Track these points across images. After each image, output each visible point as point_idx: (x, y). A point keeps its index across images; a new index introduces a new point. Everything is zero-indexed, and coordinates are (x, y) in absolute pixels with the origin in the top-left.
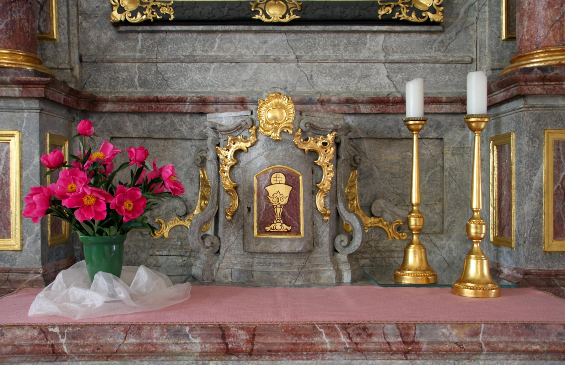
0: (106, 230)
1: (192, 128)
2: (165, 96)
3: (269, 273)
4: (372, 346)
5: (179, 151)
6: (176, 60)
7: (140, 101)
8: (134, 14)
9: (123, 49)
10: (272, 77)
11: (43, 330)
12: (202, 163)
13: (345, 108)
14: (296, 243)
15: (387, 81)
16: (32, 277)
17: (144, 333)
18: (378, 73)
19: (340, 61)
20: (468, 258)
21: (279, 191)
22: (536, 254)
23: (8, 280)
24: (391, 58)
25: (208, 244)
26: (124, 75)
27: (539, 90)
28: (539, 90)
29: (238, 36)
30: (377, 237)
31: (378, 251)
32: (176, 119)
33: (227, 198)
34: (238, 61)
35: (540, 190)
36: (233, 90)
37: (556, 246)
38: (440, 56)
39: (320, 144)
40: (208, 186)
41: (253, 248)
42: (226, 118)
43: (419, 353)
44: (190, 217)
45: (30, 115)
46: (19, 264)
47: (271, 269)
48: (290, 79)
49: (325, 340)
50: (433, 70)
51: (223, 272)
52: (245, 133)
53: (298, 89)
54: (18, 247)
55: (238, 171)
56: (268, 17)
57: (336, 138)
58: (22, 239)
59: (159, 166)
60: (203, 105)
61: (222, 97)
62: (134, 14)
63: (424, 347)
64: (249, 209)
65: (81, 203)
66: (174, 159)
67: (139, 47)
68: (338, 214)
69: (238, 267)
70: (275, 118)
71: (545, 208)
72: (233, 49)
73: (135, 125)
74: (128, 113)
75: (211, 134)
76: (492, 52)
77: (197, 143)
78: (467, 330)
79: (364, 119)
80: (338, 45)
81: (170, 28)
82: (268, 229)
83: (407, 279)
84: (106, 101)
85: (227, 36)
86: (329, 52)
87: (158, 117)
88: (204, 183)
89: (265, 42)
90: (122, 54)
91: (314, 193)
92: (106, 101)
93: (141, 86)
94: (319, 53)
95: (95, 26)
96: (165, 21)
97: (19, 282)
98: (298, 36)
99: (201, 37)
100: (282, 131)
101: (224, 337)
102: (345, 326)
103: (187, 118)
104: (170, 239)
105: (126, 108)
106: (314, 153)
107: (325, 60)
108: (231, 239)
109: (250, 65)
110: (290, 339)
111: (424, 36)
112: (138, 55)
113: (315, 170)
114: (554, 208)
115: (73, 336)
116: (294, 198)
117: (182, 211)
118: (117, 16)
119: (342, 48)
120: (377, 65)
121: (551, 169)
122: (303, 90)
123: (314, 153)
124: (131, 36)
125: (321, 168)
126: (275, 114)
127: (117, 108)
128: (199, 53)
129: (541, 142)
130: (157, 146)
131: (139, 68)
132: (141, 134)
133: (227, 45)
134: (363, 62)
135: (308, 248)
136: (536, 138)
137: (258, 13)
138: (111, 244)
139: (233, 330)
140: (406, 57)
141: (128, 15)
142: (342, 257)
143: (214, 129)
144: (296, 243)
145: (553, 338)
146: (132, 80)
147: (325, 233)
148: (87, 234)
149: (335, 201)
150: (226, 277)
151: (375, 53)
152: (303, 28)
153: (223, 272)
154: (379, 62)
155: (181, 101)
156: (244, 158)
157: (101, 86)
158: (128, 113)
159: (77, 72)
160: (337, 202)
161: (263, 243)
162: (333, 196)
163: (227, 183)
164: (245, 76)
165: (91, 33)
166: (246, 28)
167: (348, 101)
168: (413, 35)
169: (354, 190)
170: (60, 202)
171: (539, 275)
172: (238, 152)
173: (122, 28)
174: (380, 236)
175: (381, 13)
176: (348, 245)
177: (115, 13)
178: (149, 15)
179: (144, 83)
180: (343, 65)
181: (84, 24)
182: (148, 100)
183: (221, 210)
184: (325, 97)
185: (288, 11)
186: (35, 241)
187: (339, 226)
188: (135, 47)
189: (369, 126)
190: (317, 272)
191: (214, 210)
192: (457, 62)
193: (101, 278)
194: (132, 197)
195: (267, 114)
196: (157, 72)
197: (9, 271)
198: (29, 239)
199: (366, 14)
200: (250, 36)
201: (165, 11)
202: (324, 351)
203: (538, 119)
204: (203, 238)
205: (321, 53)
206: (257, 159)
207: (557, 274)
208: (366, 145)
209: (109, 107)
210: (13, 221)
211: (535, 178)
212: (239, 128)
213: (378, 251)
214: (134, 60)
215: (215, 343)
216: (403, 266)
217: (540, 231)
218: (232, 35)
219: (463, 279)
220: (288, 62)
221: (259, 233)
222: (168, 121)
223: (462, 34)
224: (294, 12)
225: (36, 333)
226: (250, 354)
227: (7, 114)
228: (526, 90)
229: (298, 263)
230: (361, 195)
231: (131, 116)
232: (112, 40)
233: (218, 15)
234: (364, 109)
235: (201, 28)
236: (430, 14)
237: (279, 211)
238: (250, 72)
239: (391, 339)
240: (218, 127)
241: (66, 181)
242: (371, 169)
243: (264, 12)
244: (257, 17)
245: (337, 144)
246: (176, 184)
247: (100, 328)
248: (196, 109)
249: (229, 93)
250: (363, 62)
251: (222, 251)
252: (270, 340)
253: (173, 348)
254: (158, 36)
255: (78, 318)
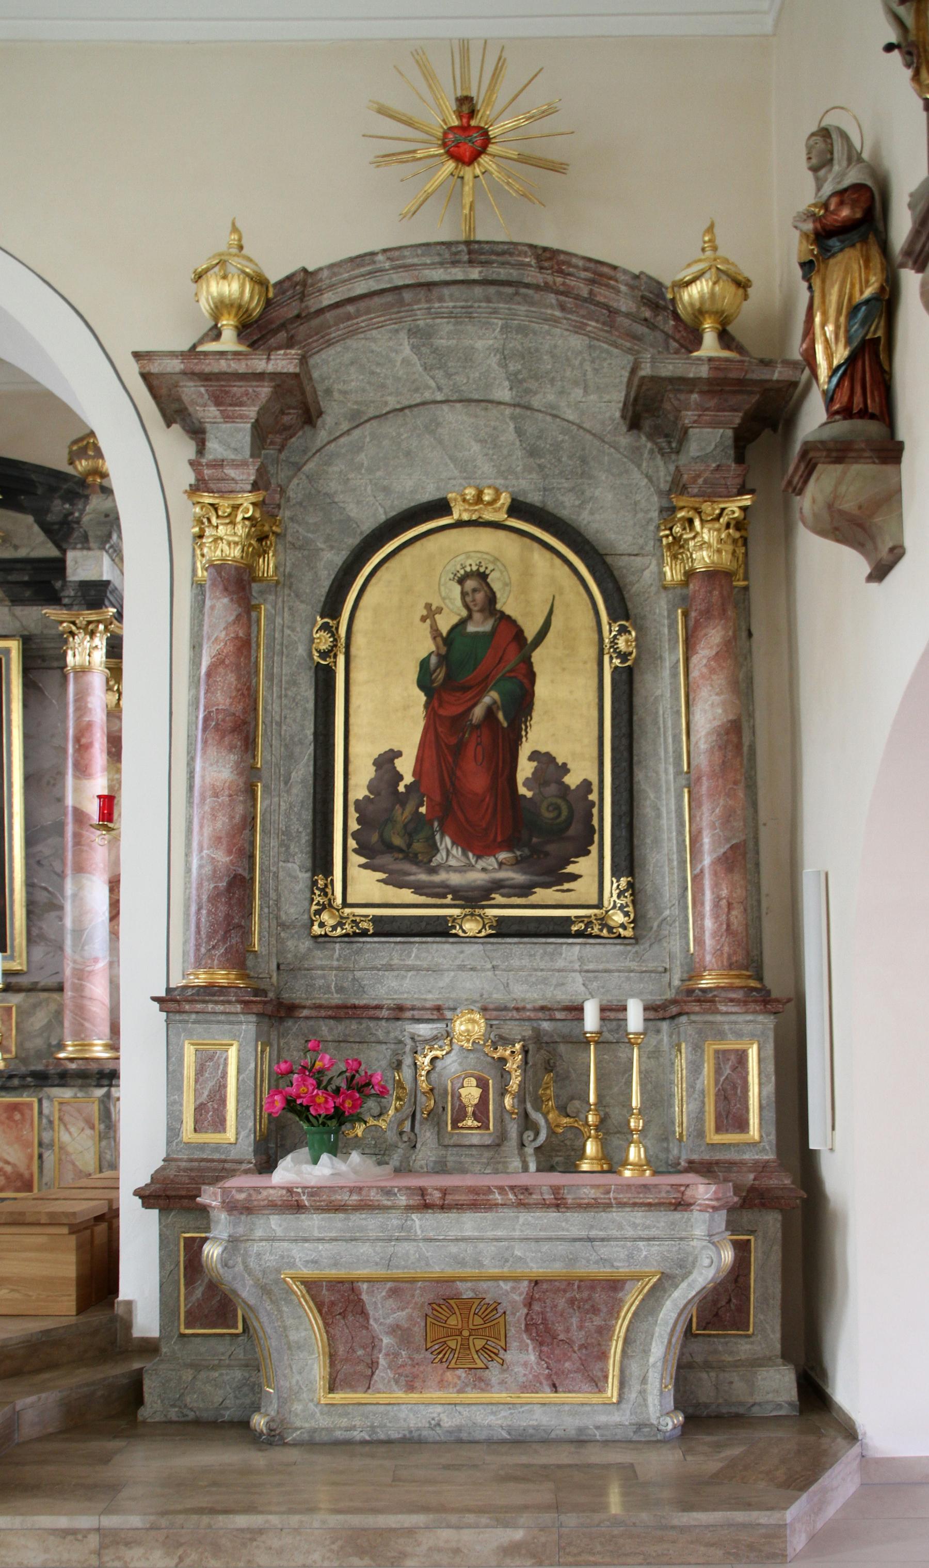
0: (329, 1122)
1: (388, 1032)
2: (362, 1002)
3: (460, 1163)
4: (531, 1201)
5: (373, 1054)
6: (372, 969)
7: (338, 1007)
8: (334, 928)
9: (320, 958)
10: (468, 985)
11: (290, 1190)
12: (398, 1066)
13: (540, 1015)
14: (486, 1138)
15: (583, 988)
16: (245, 1166)
17: (364, 1193)
18: (573, 981)
19: (536, 970)
20: (629, 1147)
21: (471, 1093)
22: (700, 1146)
23: (223, 1169)
24: (586, 968)
25: (405, 1139)
26: (321, 982)
27: (697, 1009)
28: (697, 1009)
29: (435, 946)
30: (572, 1136)
31: (573, 1150)
32: (372, 1024)
33: (424, 1098)
34: (435, 970)
35: (703, 1092)
36: (430, 996)
37: (718, 1138)
38: (633, 965)
39: (508, 1052)
40: (404, 1088)
41: (446, 1142)
42: (424, 1030)
43: (568, 1208)
44: (385, 1117)
45: (248, 1027)
46: (233, 1154)
47: (463, 1159)
48: (486, 986)
49: (498, 1197)
50: (628, 979)
51: (419, 1163)
52: (440, 1043)
53: (495, 996)
54: (233, 1140)
55: (434, 1076)
56: (464, 931)
57: (523, 1046)
58: (237, 1134)
59: (369, 1073)
60: (399, 1012)
61: (418, 1004)
62: (334, 928)
63: (569, 1201)
64: (444, 1108)
65: (314, 1101)
66: (375, 1062)
67: (336, 955)
68: (526, 1115)
69: (433, 1159)
70: (468, 1031)
71: (707, 1108)
72: (430, 958)
73: (331, 1029)
74: (325, 1018)
75: (409, 1042)
76: (682, 965)
77: (393, 1046)
78: (601, 1190)
79: (560, 1024)
80: (534, 955)
81: (368, 939)
82: (460, 1125)
83: (585, 1167)
84: (304, 1007)
85: (424, 946)
86: (525, 962)
87: (354, 1022)
88: (400, 1085)
89: (462, 952)
90: (319, 963)
91: (503, 1095)
92: (304, 1007)
93: (337, 992)
94: (515, 963)
95: (293, 937)
96: (364, 933)
97: (234, 1170)
98: (495, 947)
99: (398, 947)
100: (474, 1042)
101: (423, 1195)
102: (512, 1188)
103: (383, 1023)
104: (364, 1138)
105: (323, 1013)
106: (503, 1060)
107: (522, 969)
108: (427, 1135)
109: (446, 974)
110: (471, 1197)
111: (618, 947)
112: (335, 963)
113: (504, 1075)
114: (716, 1107)
115: (311, 1195)
116: (484, 1099)
117: (376, 1111)
118: (316, 930)
119: (538, 958)
120: (573, 974)
121: (712, 1074)
122: (499, 997)
123: (503, 1060)
124: (328, 945)
125: (509, 1073)
126: (468, 1026)
127: (314, 1013)
128: (395, 961)
129: (703, 1051)
130: (352, 1048)
131: (336, 976)
132: (336, 1038)
133: (424, 955)
134: (559, 971)
135: (497, 1141)
136: (697, 1048)
137: (454, 927)
138: (329, 1133)
139: (430, 1191)
140: (601, 967)
141: (328, 929)
142: (529, 1150)
143: (413, 1039)
144: (486, 1138)
145: (663, 1195)
146: (329, 987)
147: (513, 1130)
148: (313, 1125)
149: (522, 1101)
150: (422, 1167)
151: (571, 962)
152: (499, 940)
153: (419, 1163)
154: (574, 971)
155: (378, 1007)
156: (439, 1064)
157: (297, 993)
158: (325, 1018)
159: (274, 979)
160: (525, 1102)
161: (456, 1137)
162: (521, 1097)
163: (424, 1085)
164: (441, 984)
165: (289, 943)
166: (443, 939)
167: (543, 1008)
168: (608, 947)
169: (548, 1092)
170: (295, 1101)
171: (701, 1163)
172: (434, 1059)
173: (320, 940)
174: (576, 1135)
175: (574, 928)
176: (534, 1140)
177: (316, 927)
178: (348, 928)
179: (340, 990)
180: (539, 974)
181: (282, 935)
182: (345, 1007)
183: (418, 1109)
184: (521, 1005)
185: (484, 927)
186: (248, 1136)
187: (527, 1123)
188: (332, 956)
189: (565, 1031)
190: (505, 1162)
191: (411, 1110)
192: (651, 972)
193: (325, 1157)
194: (351, 1097)
195: (460, 1027)
196: (354, 979)
197: (225, 1161)
198: (243, 1134)
199: (560, 929)
200: (447, 946)
201: (364, 925)
202: (496, 1205)
203: (700, 1032)
204: (401, 1133)
205: (518, 963)
206: (452, 1065)
207: (717, 1163)
208: (562, 1048)
209: (305, 1013)
210: (228, 1118)
211: (698, 1082)
212: (435, 1038)
213: (573, 1150)
214: (331, 968)
215: (416, 1200)
216: (582, 1155)
217: (703, 1125)
218: (429, 946)
219: (625, 1163)
220: (483, 970)
221: (452, 1128)
222: (364, 1025)
223: (656, 947)
224: (490, 927)
225: (284, 1192)
226: (443, 1208)
227: (227, 1027)
228: (686, 1008)
229: (487, 1154)
230: (557, 1097)
231: (327, 1021)
232: (309, 949)
233: (416, 929)
234: (558, 1015)
235: (399, 939)
236: (621, 930)
237: (470, 1110)
238: (447, 980)
239: (546, 1197)
240: (417, 1038)
241: (298, 1086)
242: (569, 1072)
243: (461, 927)
244: (454, 931)
245: (525, 1051)
246: (383, 1087)
247: (332, 1189)
248: (392, 1014)
249: (425, 1000)
250: (559, 971)
251: (418, 1146)
252: (457, 1197)
253: (386, 1202)
254: (355, 946)
255: (312, 1184)
